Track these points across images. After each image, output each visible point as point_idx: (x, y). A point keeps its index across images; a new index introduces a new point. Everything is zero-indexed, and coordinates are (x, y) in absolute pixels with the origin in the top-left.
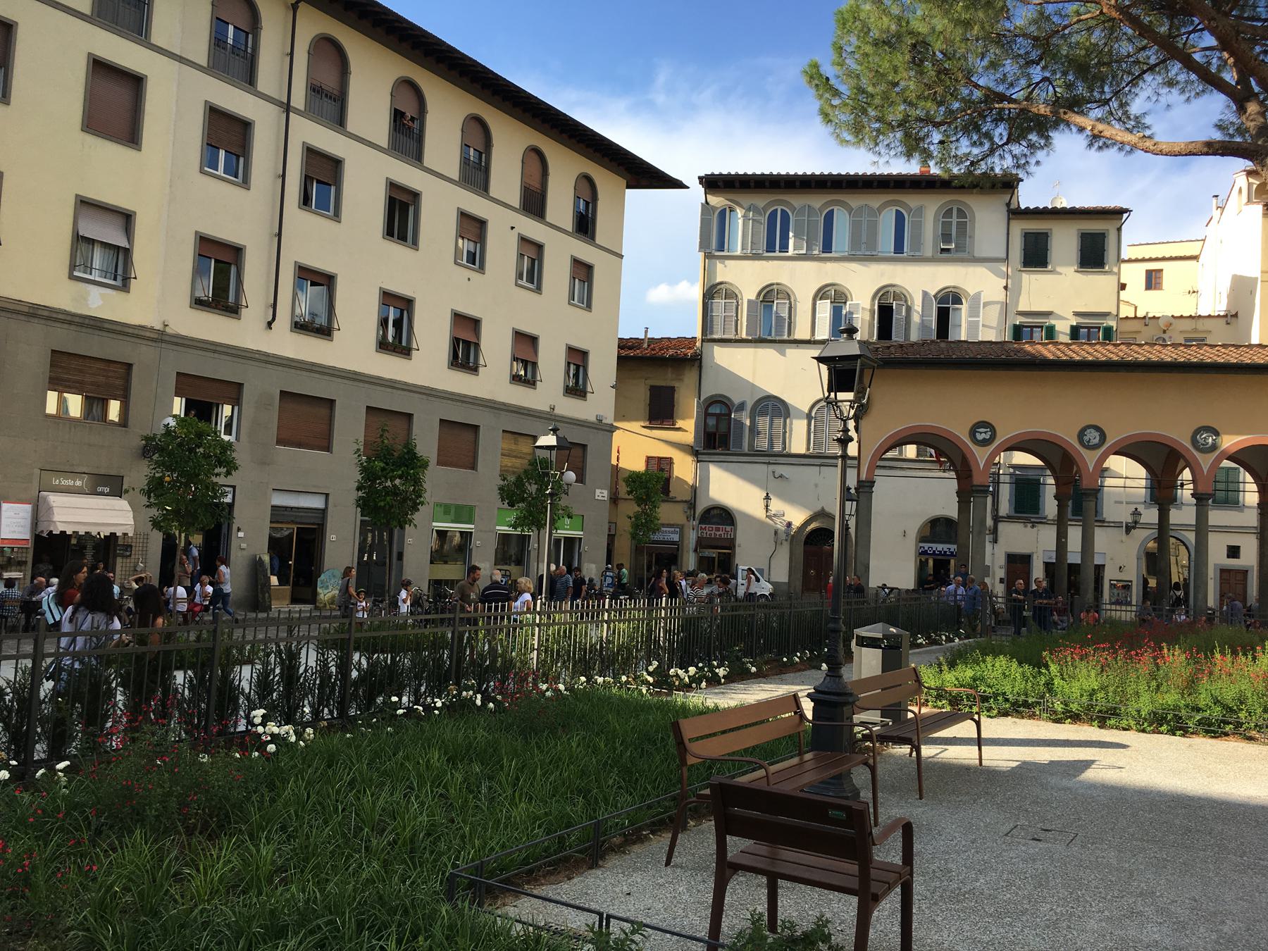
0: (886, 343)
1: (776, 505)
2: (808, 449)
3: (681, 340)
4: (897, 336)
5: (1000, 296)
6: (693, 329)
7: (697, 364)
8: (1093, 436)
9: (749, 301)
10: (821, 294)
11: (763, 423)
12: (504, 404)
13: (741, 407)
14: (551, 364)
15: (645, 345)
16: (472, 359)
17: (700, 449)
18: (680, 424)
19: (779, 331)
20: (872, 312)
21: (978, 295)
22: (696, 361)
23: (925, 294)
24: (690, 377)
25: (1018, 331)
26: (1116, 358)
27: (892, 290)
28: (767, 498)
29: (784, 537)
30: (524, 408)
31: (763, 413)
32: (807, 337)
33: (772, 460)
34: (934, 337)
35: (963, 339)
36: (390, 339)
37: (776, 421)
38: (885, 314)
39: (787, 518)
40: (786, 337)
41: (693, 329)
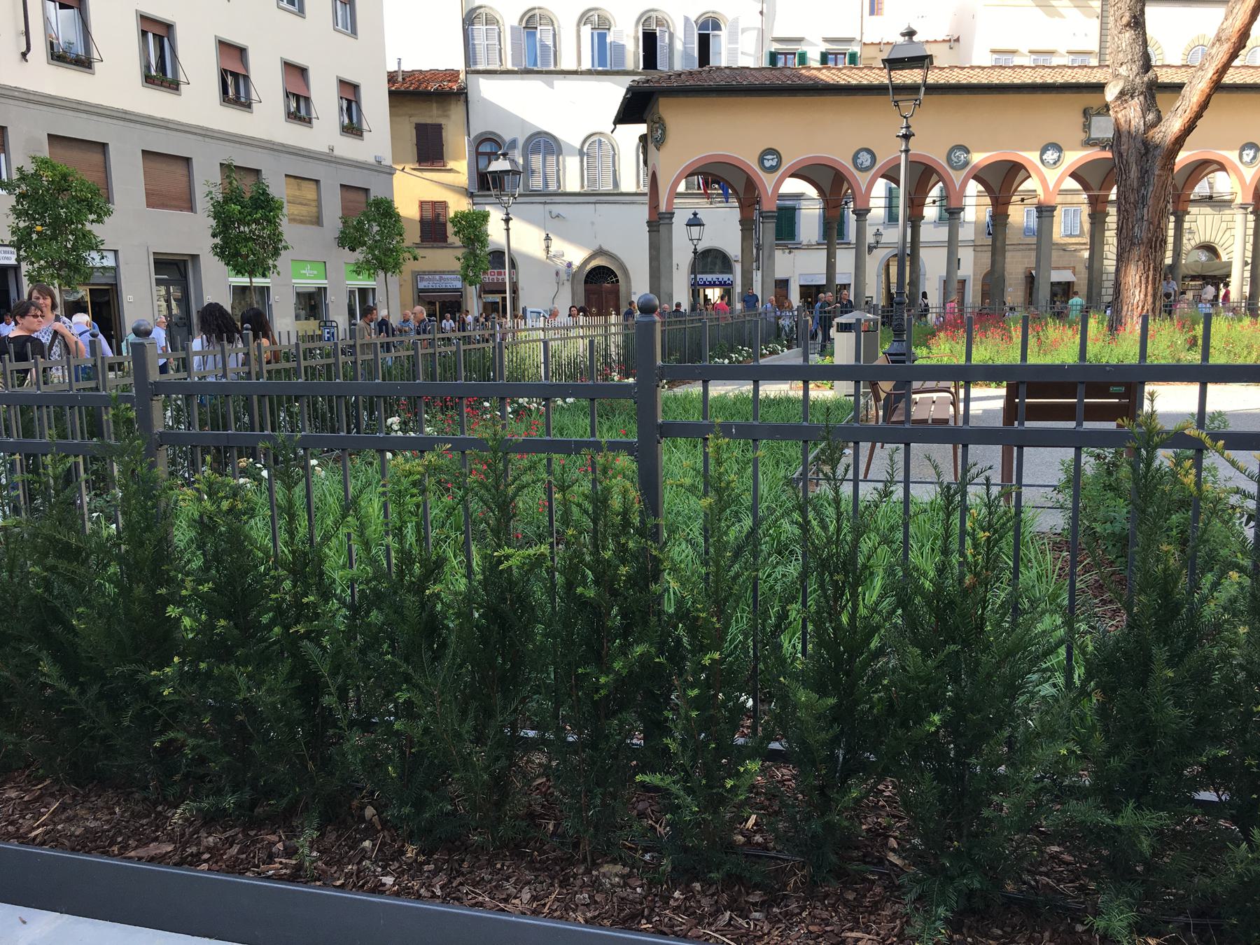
0: (653, 75)
1: (557, 245)
2: (582, 186)
3: (434, 74)
4: (662, 64)
5: (757, 21)
6: (456, 62)
7: (463, 98)
8: (865, 159)
9: (512, 28)
10: (584, 18)
11: (536, 161)
12: (283, 145)
13: (513, 144)
14: (325, 100)
15: (400, 79)
16: (242, 93)
17: (475, 191)
18: (451, 165)
19: (545, 61)
20: (637, 39)
21: (736, 20)
22: (462, 95)
23: (687, 19)
24: (456, 111)
25: (773, 57)
26: (854, 82)
27: (654, 14)
28: (548, 238)
29: (565, 277)
30: (304, 150)
31: (536, 151)
32: (573, 67)
33: (547, 199)
34: (696, 66)
35: (724, 64)
36: (153, 73)
37: (549, 158)
38: (650, 40)
39: (567, 258)
40: (552, 68)
41: (456, 62)
